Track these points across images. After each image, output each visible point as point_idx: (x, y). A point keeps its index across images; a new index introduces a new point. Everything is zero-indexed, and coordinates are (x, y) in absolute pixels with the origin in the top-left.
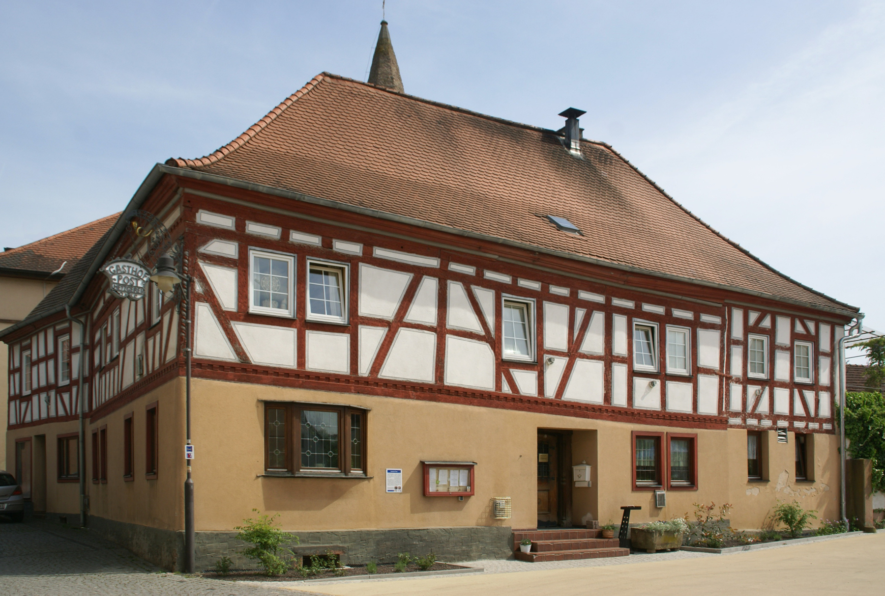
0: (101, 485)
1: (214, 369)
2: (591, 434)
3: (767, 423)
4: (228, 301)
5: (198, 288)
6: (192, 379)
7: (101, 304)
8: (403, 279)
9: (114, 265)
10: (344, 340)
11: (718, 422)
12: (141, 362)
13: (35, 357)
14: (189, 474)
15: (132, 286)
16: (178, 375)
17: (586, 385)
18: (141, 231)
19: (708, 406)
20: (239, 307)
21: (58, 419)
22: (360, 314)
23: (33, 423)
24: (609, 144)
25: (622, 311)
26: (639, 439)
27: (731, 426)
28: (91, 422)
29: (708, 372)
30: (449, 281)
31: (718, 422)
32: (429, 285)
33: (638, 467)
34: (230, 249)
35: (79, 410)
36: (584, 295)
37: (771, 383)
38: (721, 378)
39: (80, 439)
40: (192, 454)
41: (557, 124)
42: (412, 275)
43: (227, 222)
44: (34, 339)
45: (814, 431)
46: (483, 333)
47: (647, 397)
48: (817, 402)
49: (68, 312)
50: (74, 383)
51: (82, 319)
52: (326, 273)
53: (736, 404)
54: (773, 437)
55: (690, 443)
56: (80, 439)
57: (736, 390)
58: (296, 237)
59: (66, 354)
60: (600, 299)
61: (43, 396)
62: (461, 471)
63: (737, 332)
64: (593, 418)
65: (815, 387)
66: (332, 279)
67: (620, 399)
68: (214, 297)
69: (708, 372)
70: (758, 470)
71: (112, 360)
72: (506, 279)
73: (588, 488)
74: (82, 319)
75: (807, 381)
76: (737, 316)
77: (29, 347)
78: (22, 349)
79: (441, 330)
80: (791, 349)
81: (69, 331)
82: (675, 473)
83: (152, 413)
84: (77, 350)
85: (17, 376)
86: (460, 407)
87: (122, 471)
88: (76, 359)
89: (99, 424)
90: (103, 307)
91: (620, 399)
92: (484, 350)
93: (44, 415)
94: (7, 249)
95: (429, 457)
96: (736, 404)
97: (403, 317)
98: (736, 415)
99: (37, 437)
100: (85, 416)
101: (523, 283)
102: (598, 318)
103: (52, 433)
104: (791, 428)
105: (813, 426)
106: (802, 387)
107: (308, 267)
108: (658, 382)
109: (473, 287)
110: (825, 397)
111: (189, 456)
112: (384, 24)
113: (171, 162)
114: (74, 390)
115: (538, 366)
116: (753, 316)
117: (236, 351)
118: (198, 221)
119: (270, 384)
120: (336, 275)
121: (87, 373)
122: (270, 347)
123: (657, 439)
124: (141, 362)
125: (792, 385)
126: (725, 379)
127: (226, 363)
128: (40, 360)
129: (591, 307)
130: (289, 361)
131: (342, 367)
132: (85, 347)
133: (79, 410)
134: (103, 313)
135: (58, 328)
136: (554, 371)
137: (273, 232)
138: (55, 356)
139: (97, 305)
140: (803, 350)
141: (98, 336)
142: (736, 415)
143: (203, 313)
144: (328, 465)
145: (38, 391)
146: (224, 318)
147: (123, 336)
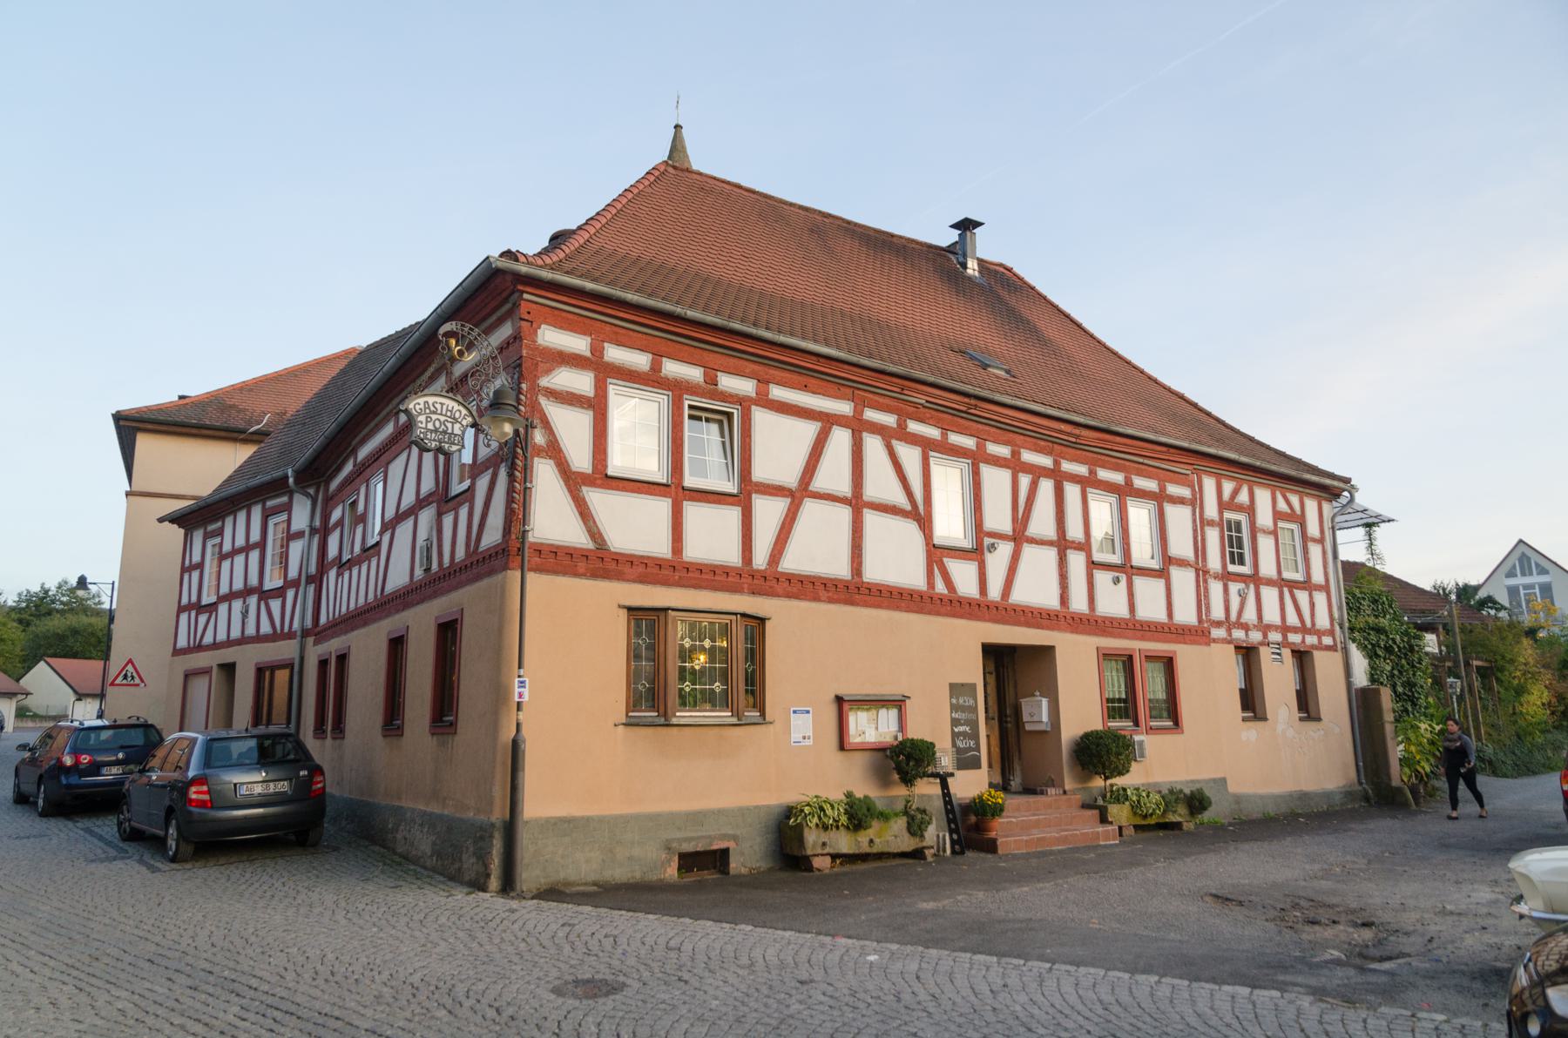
0: (329, 741)
1: (560, 560)
2: (1047, 652)
3: (1256, 636)
4: (581, 459)
5: (539, 437)
6: (531, 577)
7: (349, 467)
8: (810, 429)
9: (421, 400)
10: (733, 514)
11: (1198, 634)
12: (429, 549)
13: (227, 547)
14: (518, 725)
15: (445, 432)
16: (506, 568)
17: (1036, 583)
18: (461, 353)
19: (1186, 614)
20: (594, 466)
21: (259, 638)
22: (754, 478)
23: (215, 646)
24: (1009, 265)
25: (1075, 479)
26: (1106, 656)
27: (1214, 641)
28: (315, 643)
29: (1182, 563)
30: (865, 434)
31: (1198, 634)
32: (840, 439)
33: (1108, 700)
34: (581, 382)
35: (296, 625)
36: (1028, 456)
37: (1255, 579)
38: (1197, 570)
39: (296, 668)
40: (526, 692)
41: (948, 237)
42: (819, 424)
43: (578, 344)
44: (229, 521)
45: (1313, 647)
46: (908, 507)
47: (1112, 602)
48: (1312, 605)
49: (291, 480)
50: (295, 584)
51: (311, 491)
52: (707, 420)
53: (1218, 613)
54: (1265, 654)
55: (1169, 663)
56: (296, 668)
57: (1216, 588)
58: (672, 368)
59: (278, 543)
60: (1046, 461)
61: (237, 605)
62: (883, 712)
63: (1211, 510)
64: (1048, 628)
65: (1307, 585)
66: (714, 427)
67: (1079, 604)
68: (560, 450)
69: (1182, 563)
70: (1251, 702)
71: (365, 550)
72: (933, 432)
73: (1045, 732)
74: (311, 491)
75: (1299, 577)
76: (1209, 484)
77: (220, 532)
78: (206, 537)
79: (857, 503)
80: (1274, 533)
81: (288, 508)
82: (1153, 706)
83: (448, 632)
84: (300, 535)
85: (195, 575)
86: (883, 614)
87: (379, 719)
88: (296, 548)
89: (333, 646)
90: (351, 473)
91: (1079, 604)
92: (911, 528)
93: (236, 633)
94: (181, 397)
95: (847, 691)
96: (1218, 613)
97: (808, 484)
98: (1218, 624)
99: (221, 666)
100: (305, 633)
101: (954, 438)
102: (1046, 487)
103: (247, 660)
104: (1285, 643)
105: (1311, 640)
106: (1293, 585)
107: (686, 412)
108: (1123, 578)
109: (894, 442)
110: (1320, 598)
111: (520, 695)
112: (678, 127)
113: (508, 254)
114: (290, 594)
115: (976, 553)
116: (1228, 487)
117: (589, 531)
118: (540, 341)
119: (634, 581)
120: (720, 423)
121: (313, 569)
122: (636, 527)
123: (1128, 662)
124: (429, 549)
125: (1281, 583)
126: (1202, 573)
127: (575, 549)
128: (235, 552)
129: (1037, 473)
130: (661, 547)
131: (731, 555)
132: (313, 531)
133: (296, 625)
134: (349, 481)
135: (270, 504)
136: (998, 561)
137: (639, 360)
138: (262, 545)
139: (339, 469)
140: (1287, 534)
141: (336, 514)
142: (1218, 624)
143: (544, 475)
144: (714, 707)
145: (231, 596)
146: (573, 482)
147: (390, 513)
